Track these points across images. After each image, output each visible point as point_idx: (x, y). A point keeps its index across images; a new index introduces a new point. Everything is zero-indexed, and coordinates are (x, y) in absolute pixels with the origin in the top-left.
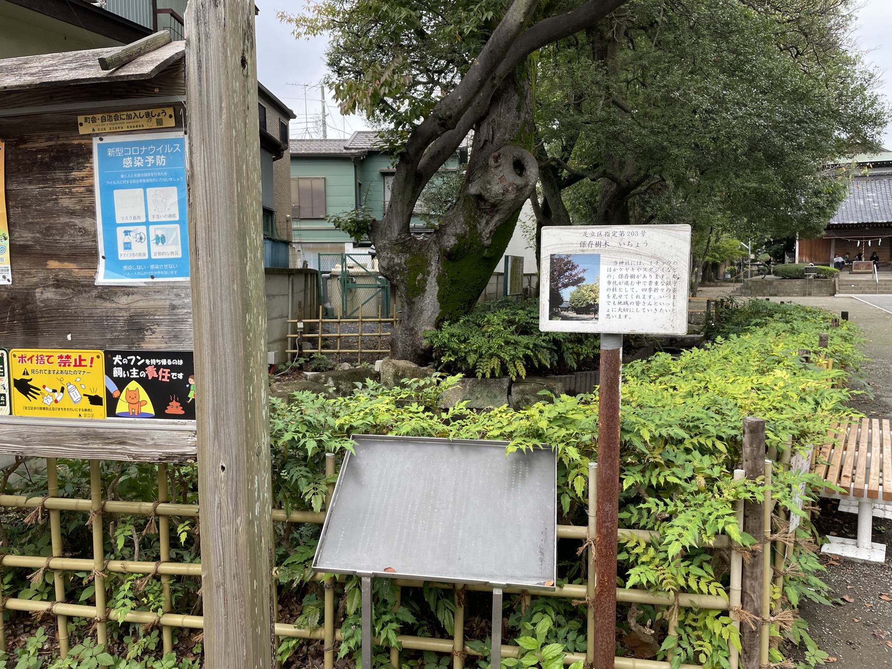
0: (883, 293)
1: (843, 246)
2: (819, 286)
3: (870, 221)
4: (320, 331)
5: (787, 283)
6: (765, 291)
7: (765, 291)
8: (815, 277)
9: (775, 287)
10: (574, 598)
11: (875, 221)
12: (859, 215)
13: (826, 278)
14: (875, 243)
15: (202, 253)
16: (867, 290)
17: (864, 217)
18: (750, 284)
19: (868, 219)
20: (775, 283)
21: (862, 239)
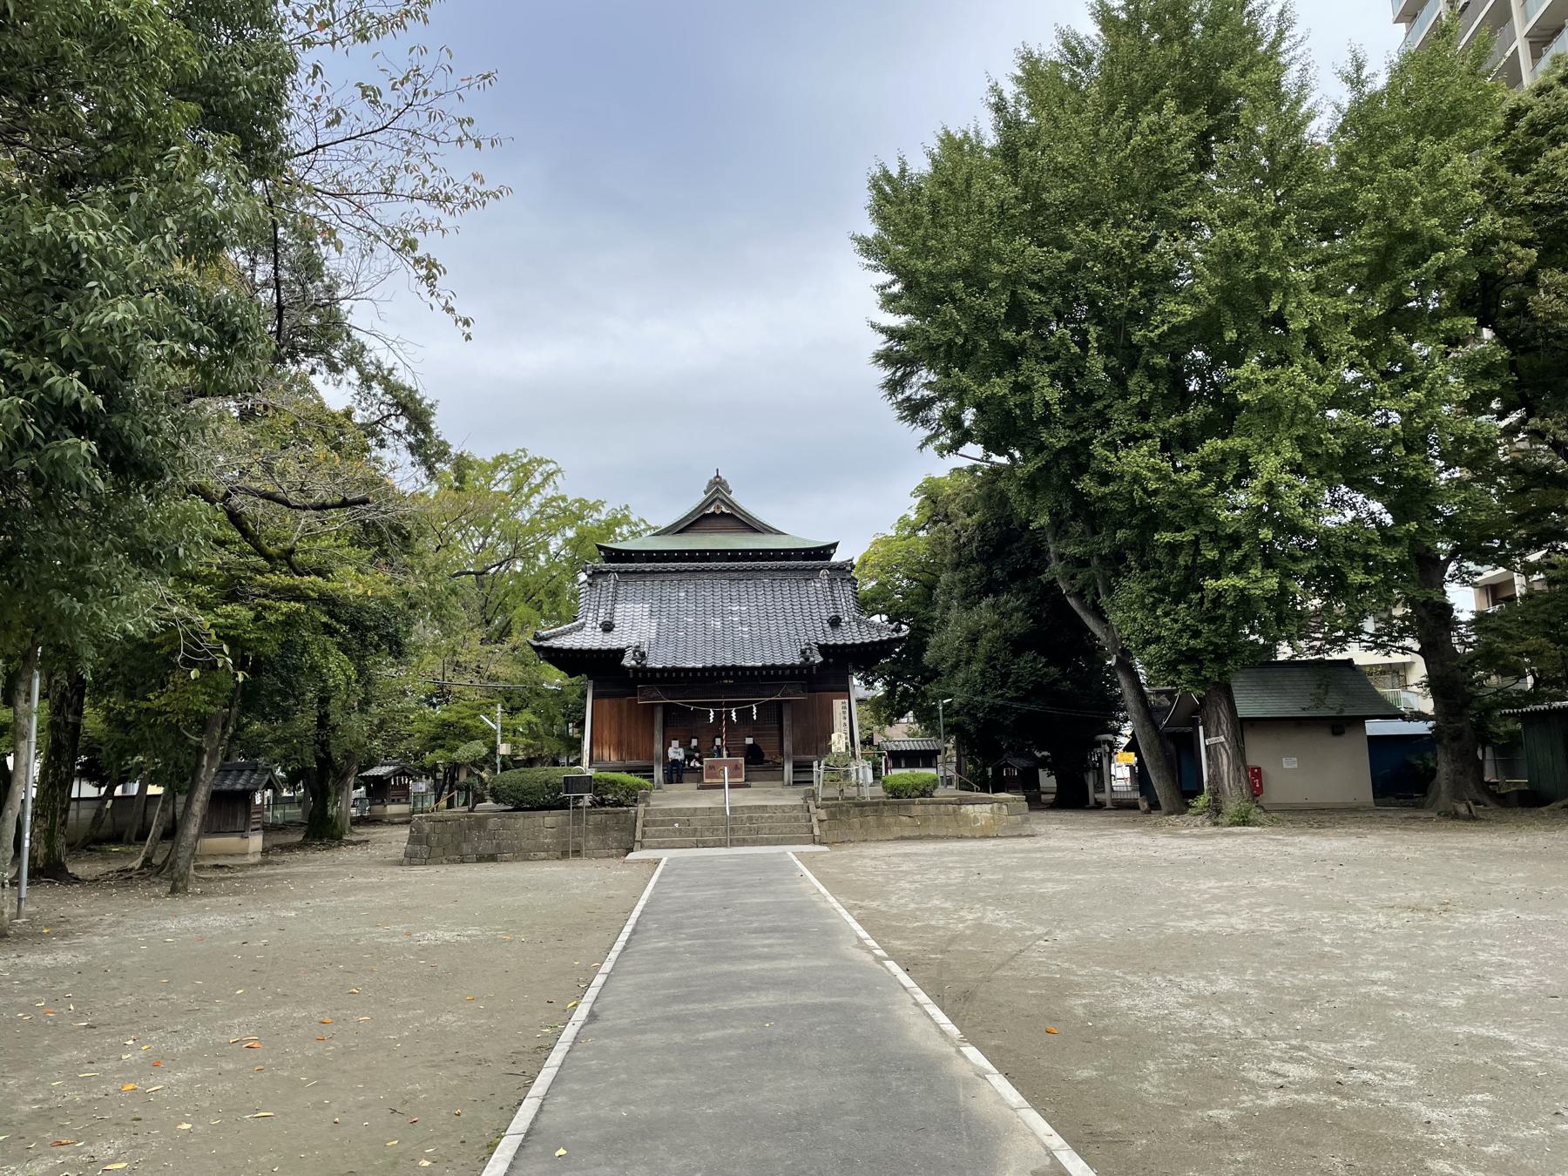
0: (743, 842)
1: (679, 722)
2: (601, 829)
3: (729, 663)
4: (1213, 740)
5: (522, 821)
6: (466, 848)
7: (466, 848)
8: (594, 804)
9: (492, 836)
10: (300, 846)
11: (739, 662)
12: (710, 652)
13: (619, 804)
14: (744, 715)
15: (220, 863)
16: (708, 837)
17: (719, 654)
18: (427, 827)
19: (727, 659)
20: (492, 823)
21: (719, 705)
